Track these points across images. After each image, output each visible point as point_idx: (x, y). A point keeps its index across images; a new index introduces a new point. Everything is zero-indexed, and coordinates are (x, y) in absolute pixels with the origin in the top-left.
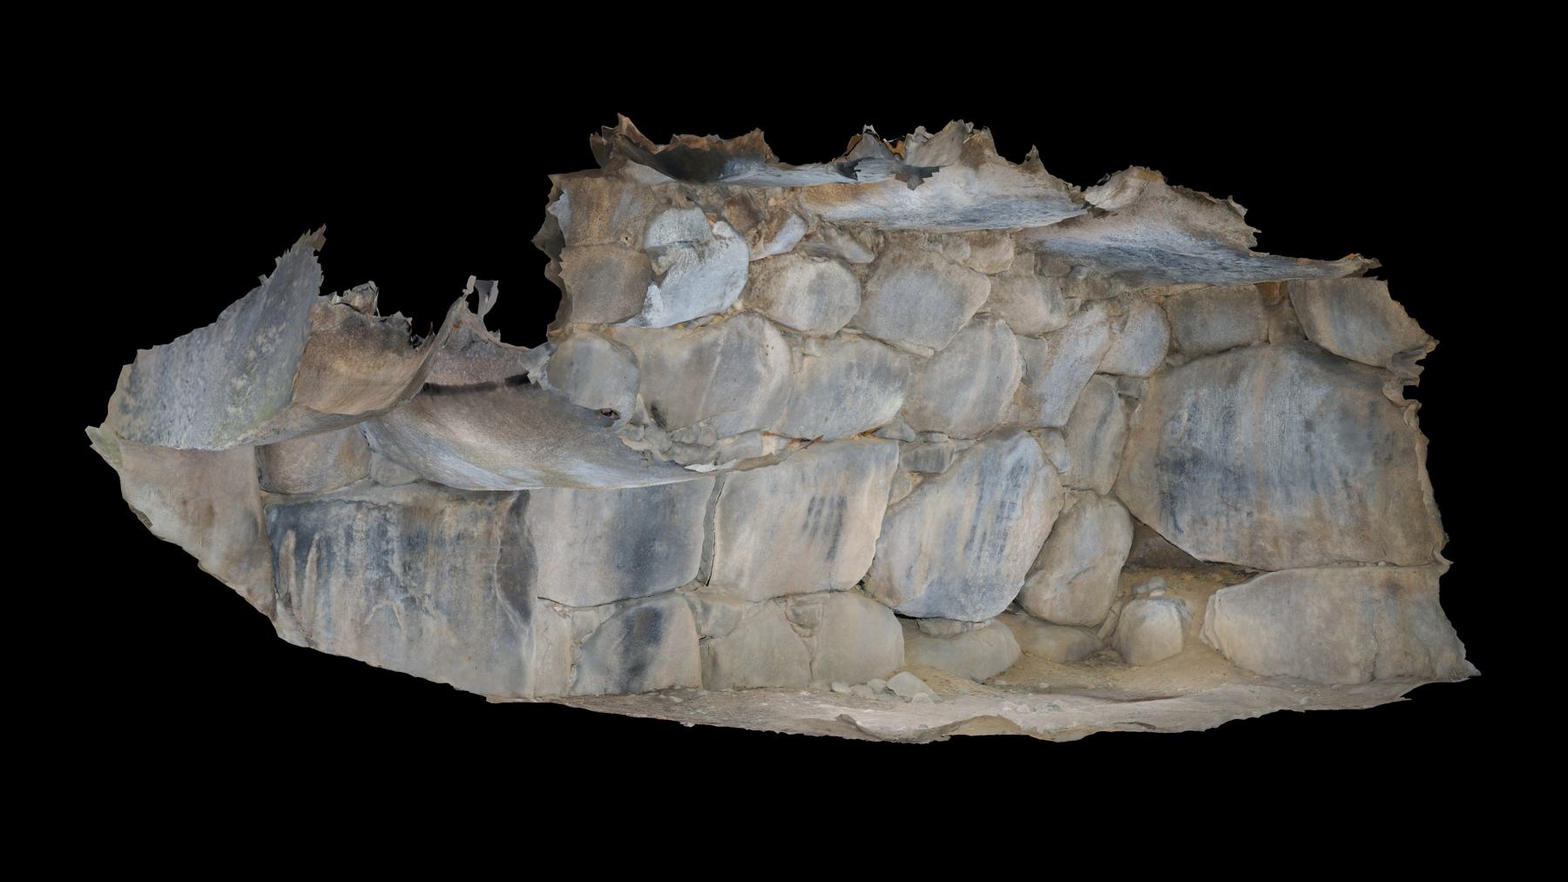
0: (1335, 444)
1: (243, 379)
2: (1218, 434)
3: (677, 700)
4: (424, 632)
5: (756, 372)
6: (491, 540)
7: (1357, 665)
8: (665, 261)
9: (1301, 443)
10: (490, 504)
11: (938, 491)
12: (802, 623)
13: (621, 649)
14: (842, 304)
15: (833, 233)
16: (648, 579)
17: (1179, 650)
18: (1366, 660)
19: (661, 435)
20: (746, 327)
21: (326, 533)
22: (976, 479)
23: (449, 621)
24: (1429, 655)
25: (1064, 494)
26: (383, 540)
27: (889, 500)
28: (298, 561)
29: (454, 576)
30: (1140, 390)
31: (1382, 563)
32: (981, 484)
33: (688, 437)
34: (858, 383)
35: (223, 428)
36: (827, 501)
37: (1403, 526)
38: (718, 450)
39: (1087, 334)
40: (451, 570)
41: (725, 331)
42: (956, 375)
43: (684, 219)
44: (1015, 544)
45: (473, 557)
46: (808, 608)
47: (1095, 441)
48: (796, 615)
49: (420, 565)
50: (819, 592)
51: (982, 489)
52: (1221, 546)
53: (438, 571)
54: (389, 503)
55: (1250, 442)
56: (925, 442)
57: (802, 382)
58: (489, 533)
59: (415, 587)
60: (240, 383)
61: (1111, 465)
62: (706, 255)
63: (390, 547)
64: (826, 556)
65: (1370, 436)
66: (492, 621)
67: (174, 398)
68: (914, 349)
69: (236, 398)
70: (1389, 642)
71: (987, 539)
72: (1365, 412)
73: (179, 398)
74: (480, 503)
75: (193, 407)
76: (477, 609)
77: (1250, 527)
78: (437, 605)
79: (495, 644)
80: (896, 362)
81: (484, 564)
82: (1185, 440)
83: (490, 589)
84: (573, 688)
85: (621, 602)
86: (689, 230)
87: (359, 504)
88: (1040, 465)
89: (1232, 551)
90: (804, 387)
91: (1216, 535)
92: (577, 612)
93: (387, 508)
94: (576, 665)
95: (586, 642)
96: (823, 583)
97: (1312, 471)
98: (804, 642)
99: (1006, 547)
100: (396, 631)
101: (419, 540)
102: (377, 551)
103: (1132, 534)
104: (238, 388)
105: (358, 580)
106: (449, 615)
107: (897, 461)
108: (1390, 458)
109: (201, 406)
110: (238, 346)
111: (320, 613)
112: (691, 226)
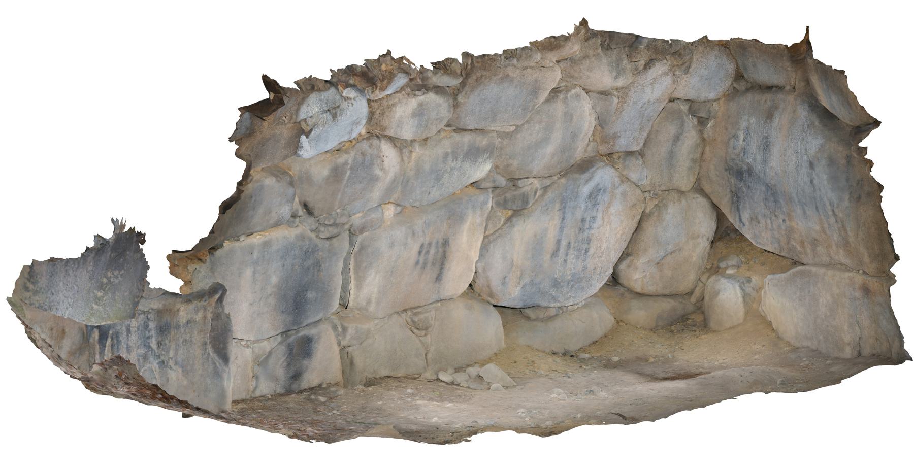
0: (826, 182)
1: (101, 292)
3: (322, 399)
4: (170, 379)
5: (376, 175)
6: (206, 321)
7: (849, 344)
8: (311, 121)
9: (808, 176)
10: (205, 301)
11: (524, 222)
12: (419, 327)
13: (285, 364)
14: (439, 117)
16: (303, 316)
17: (742, 321)
18: (854, 341)
19: (311, 220)
20: (367, 148)
21: (116, 330)
22: (557, 206)
23: (183, 371)
24: (888, 342)
25: (645, 198)
26: (146, 330)
27: (485, 233)
28: (101, 346)
29: (185, 345)
30: (709, 111)
31: (861, 271)
32: (563, 209)
33: (329, 221)
35: (91, 315)
36: (433, 244)
37: (868, 248)
38: (351, 223)
39: (652, 84)
40: (183, 342)
41: (353, 154)
42: (534, 140)
43: (323, 97)
44: (599, 245)
45: (196, 332)
46: (422, 316)
47: (671, 155)
48: (414, 322)
49: (167, 342)
50: (431, 303)
51: (564, 213)
52: (770, 242)
53: (176, 343)
54: (149, 310)
55: (779, 168)
56: (514, 186)
57: (411, 170)
59: (164, 354)
60: (99, 294)
61: (690, 169)
62: (338, 115)
63: (150, 334)
64: (434, 280)
65: (847, 180)
66: (207, 368)
67: (59, 291)
68: (498, 129)
69: (97, 301)
70: (867, 329)
71: (572, 247)
72: (844, 162)
73: (62, 292)
74: (200, 302)
75: (71, 298)
76: (199, 362)
78: (176, 363)
79: (209, 381)
80: (482, 141)
81: (202, 336)
82: (742, 155)
83: (206, 349)
84: (254, 392)
85: (285, 333)
86: (326, 103)
88: (617, 185)
89: (776, 245)
90: (412, 173)
91: (766, 232)
92: (255, 344)
93: (148, 312)
94: (256, 377)
95: (262, 361)
96: (434, 297)
97: (815, 198)
98: (421, 341)
99: (590, 249)
101: (166, 328)
102: (144, 338)
103: (715, 219)
104: (98, 296)
106: (183, 368)
107: (490, 205)
108: (859, 198)
109: (75, 299)
110: (96, 273)
112: (327, 100)
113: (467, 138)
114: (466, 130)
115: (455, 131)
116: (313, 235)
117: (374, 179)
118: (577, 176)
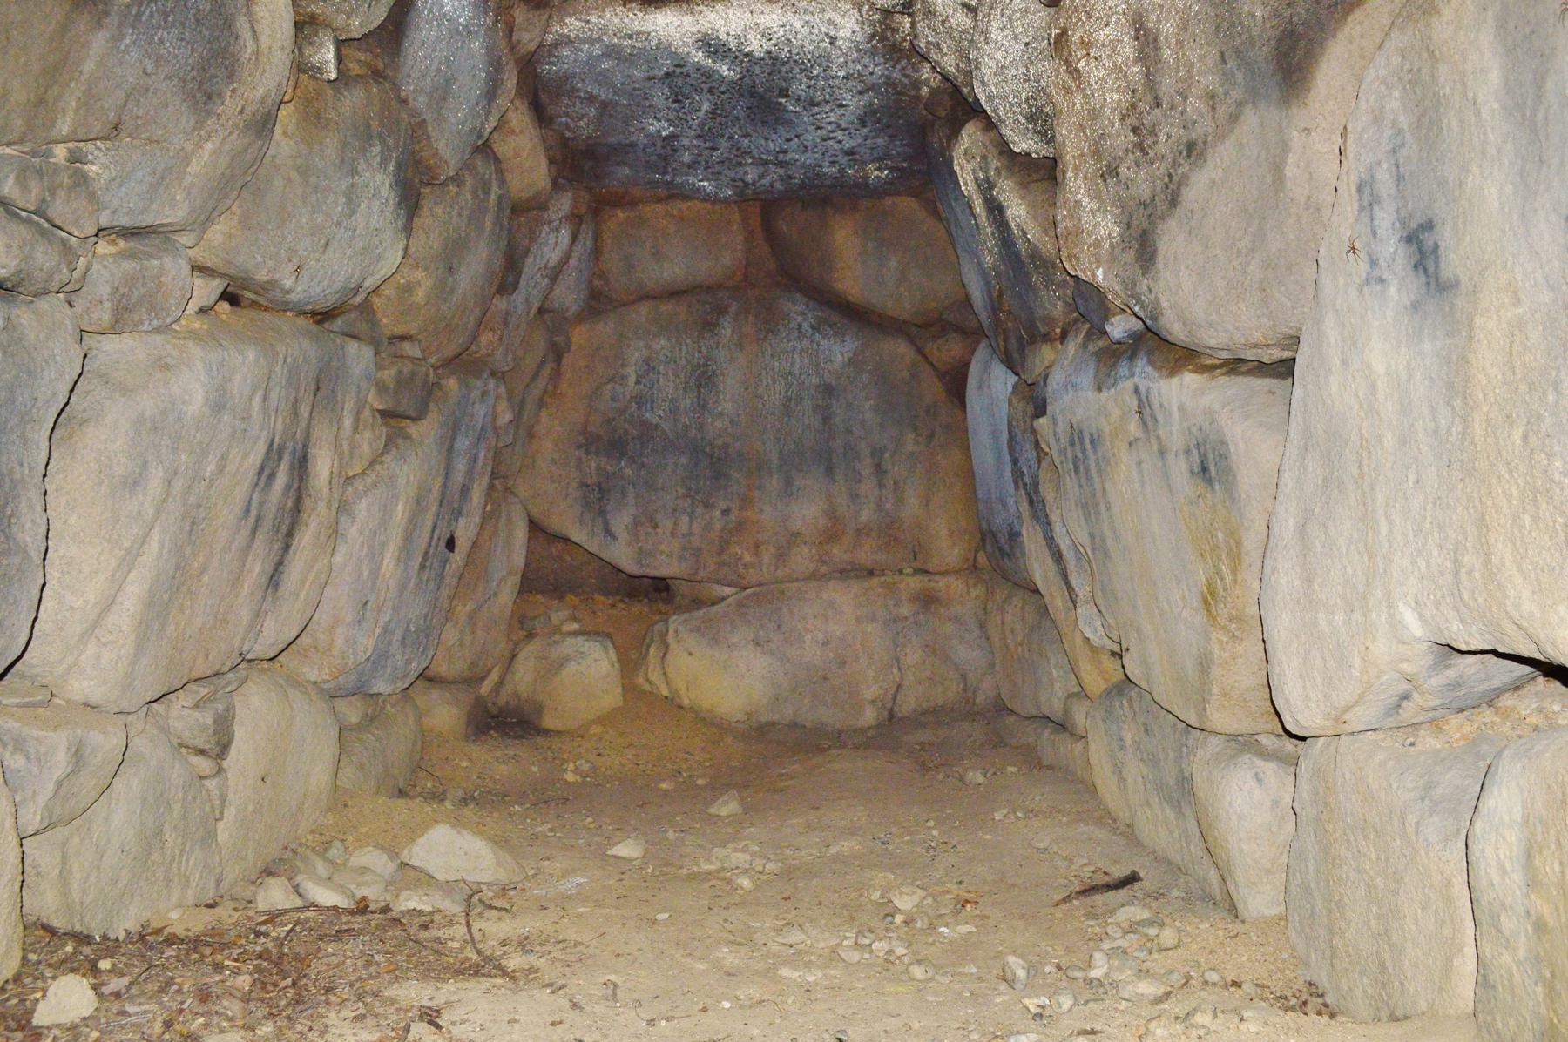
2: (688, 401)
7: (873, 702)
77: (722, 530)
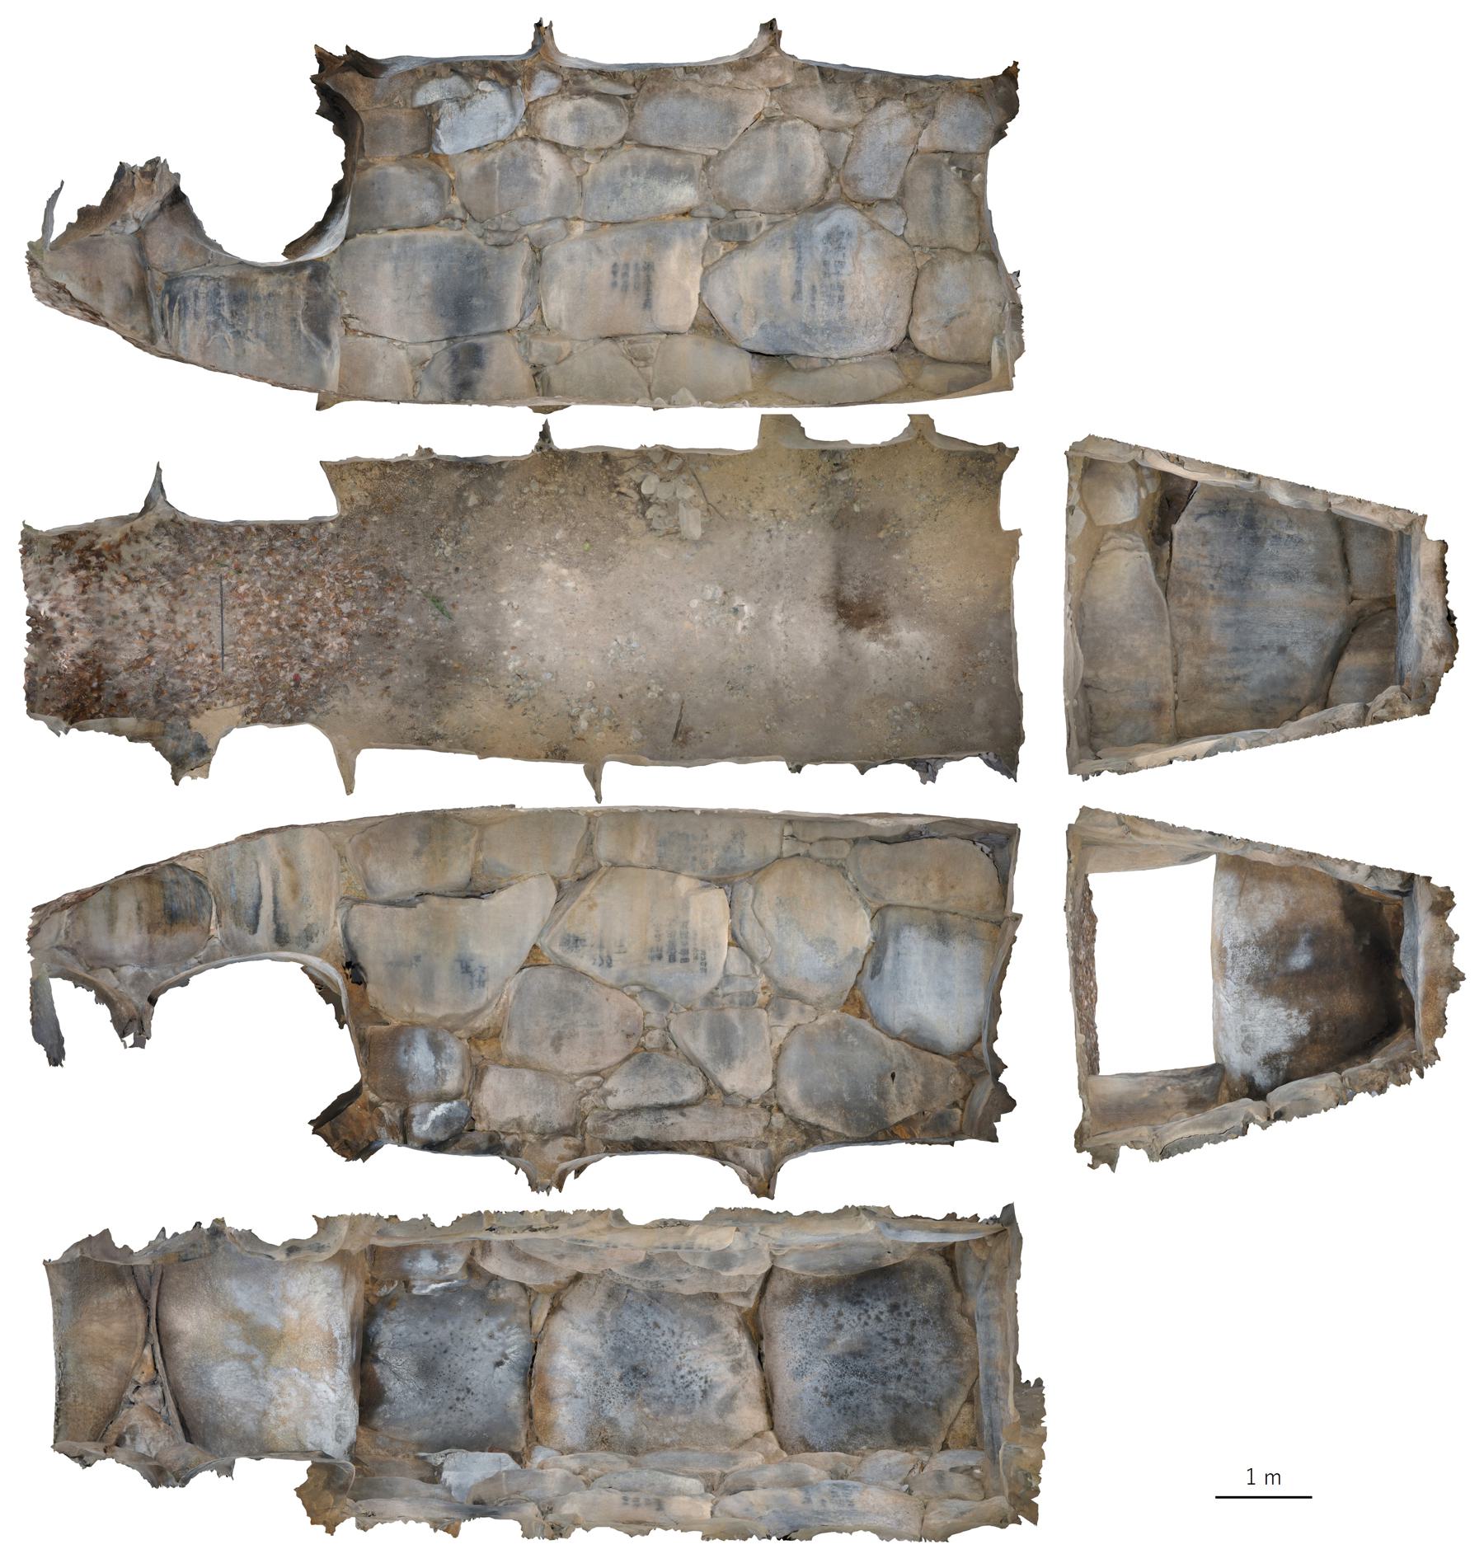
13: (450, 371)
15: (588, 78)
34: (634, 180)
41: (500, 153)
47: (938, 209)
51: (800, 252)
58: (292, 293)
79: (301, 359)
87: (202, 278)
93: (219, 279)
98: (640, 372)
100: (227, 350)
105: (202, 321)
111: (181, 340)
113: (649, 154)
114: (650, 147)
115: (636, 146)
116: (481, 242)
117: (532, 184)
118: (811, 214)
